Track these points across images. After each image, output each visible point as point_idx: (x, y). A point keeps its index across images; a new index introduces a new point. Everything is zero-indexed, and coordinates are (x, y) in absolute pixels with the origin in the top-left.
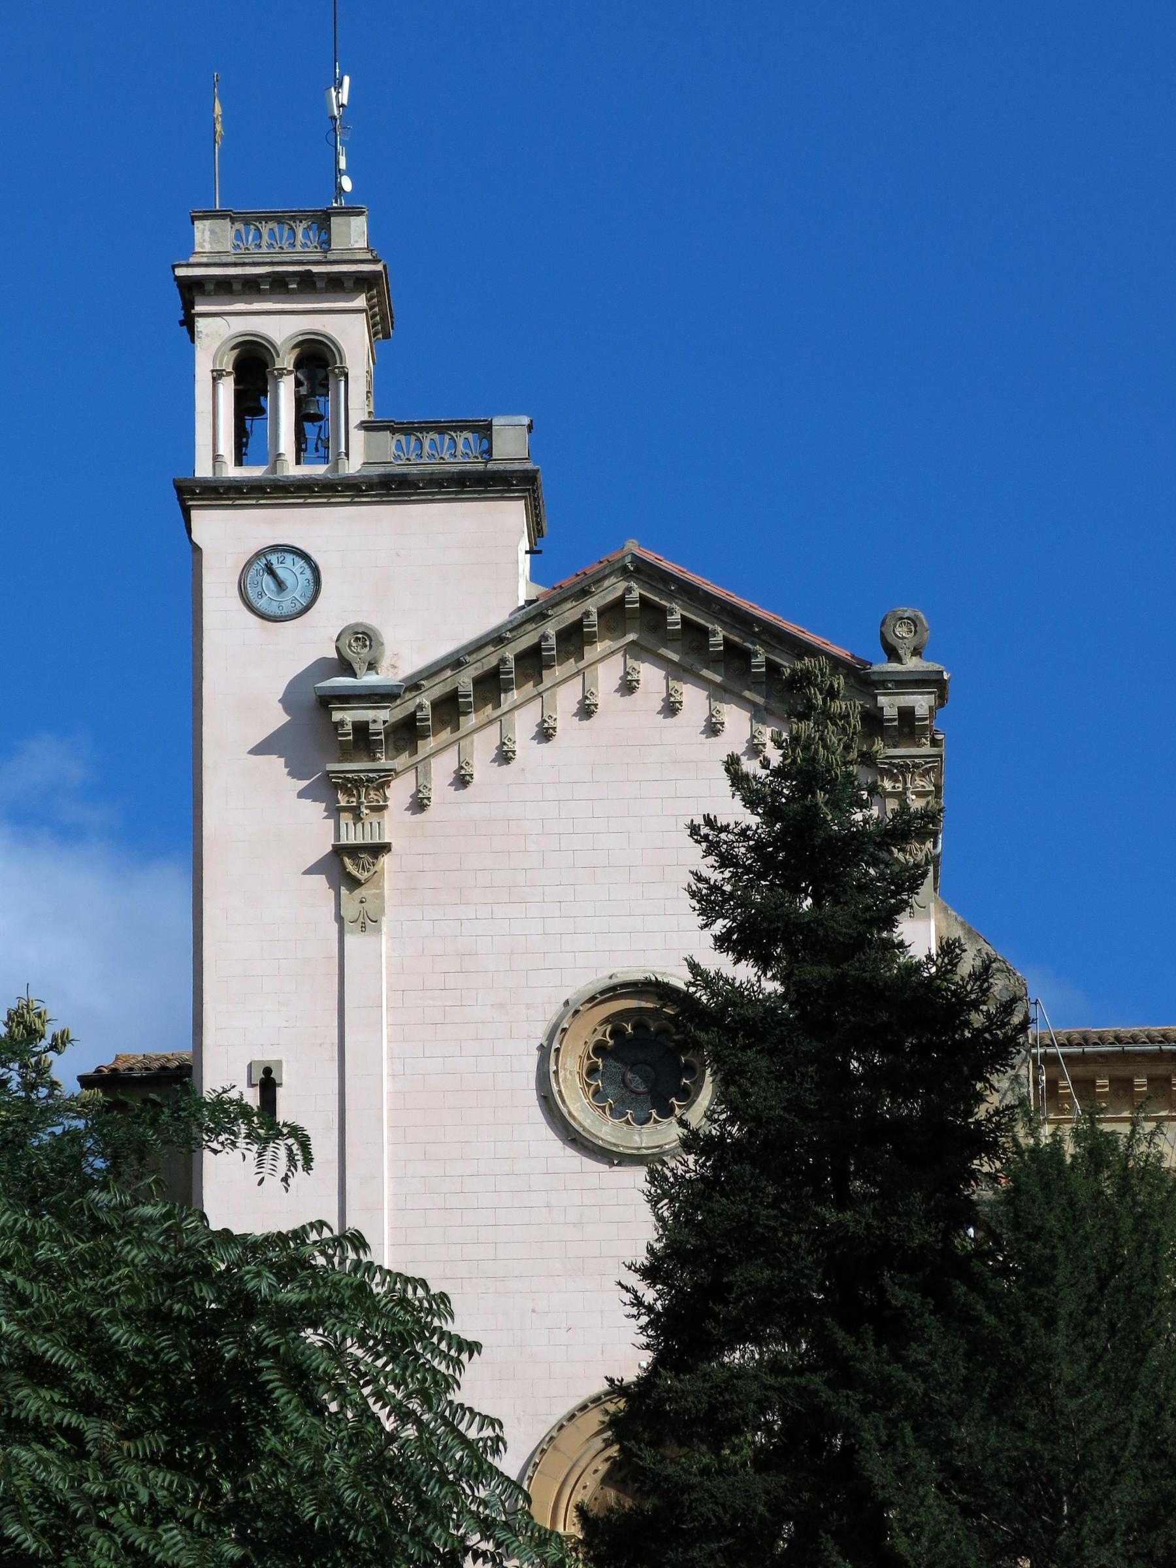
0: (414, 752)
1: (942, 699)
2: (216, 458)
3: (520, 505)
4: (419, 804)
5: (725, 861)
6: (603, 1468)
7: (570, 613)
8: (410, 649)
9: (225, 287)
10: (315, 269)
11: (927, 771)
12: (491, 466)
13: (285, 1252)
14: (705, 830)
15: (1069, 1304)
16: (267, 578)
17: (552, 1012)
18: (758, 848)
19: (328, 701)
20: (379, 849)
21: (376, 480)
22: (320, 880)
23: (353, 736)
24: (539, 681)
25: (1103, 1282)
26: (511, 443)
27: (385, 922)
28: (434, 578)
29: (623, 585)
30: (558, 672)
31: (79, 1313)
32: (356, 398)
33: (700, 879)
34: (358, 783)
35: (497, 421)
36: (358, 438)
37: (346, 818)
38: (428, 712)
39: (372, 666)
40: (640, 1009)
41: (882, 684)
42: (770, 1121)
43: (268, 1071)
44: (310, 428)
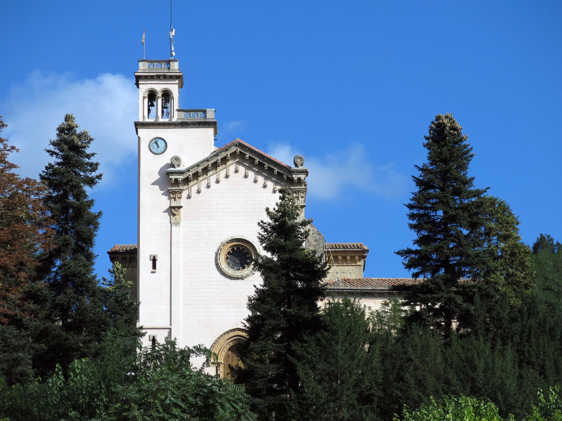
0: (188, 185)
1: (307, 175)
2: (144, 117)
4: (189, 197)
5: (266, 230)
6: (228, 347)
7: (224, 154)
8: (187, 162)
9: (146, 78)
10: (167, 74)
11: (303, 192)
12: (206, 120)
14: (261, 224)
15: (341, 338)
16: (155, 145)
17: (218, 245)
18: (272, 227)
19: (168, 174)
20: (180, 207)
22: (167, 214)
23: (174, 181)
24: (216, 169)
25: (348, 334)
26: (211, 115)
27: (181, 224)
28: (193, 146)
29: (236, 148)
30: (221, 167)
31: (183, 395)
32: (176, 103)
33: (260, 234)
34: (175, 192)
35: (208, 110)
36: (176, 113)
37: (172, 200)
38: (191, 176)
39: (179, 166)
40: (238, 245)
42: (275, 288)
43: (154, 257)
44: (165, 110)
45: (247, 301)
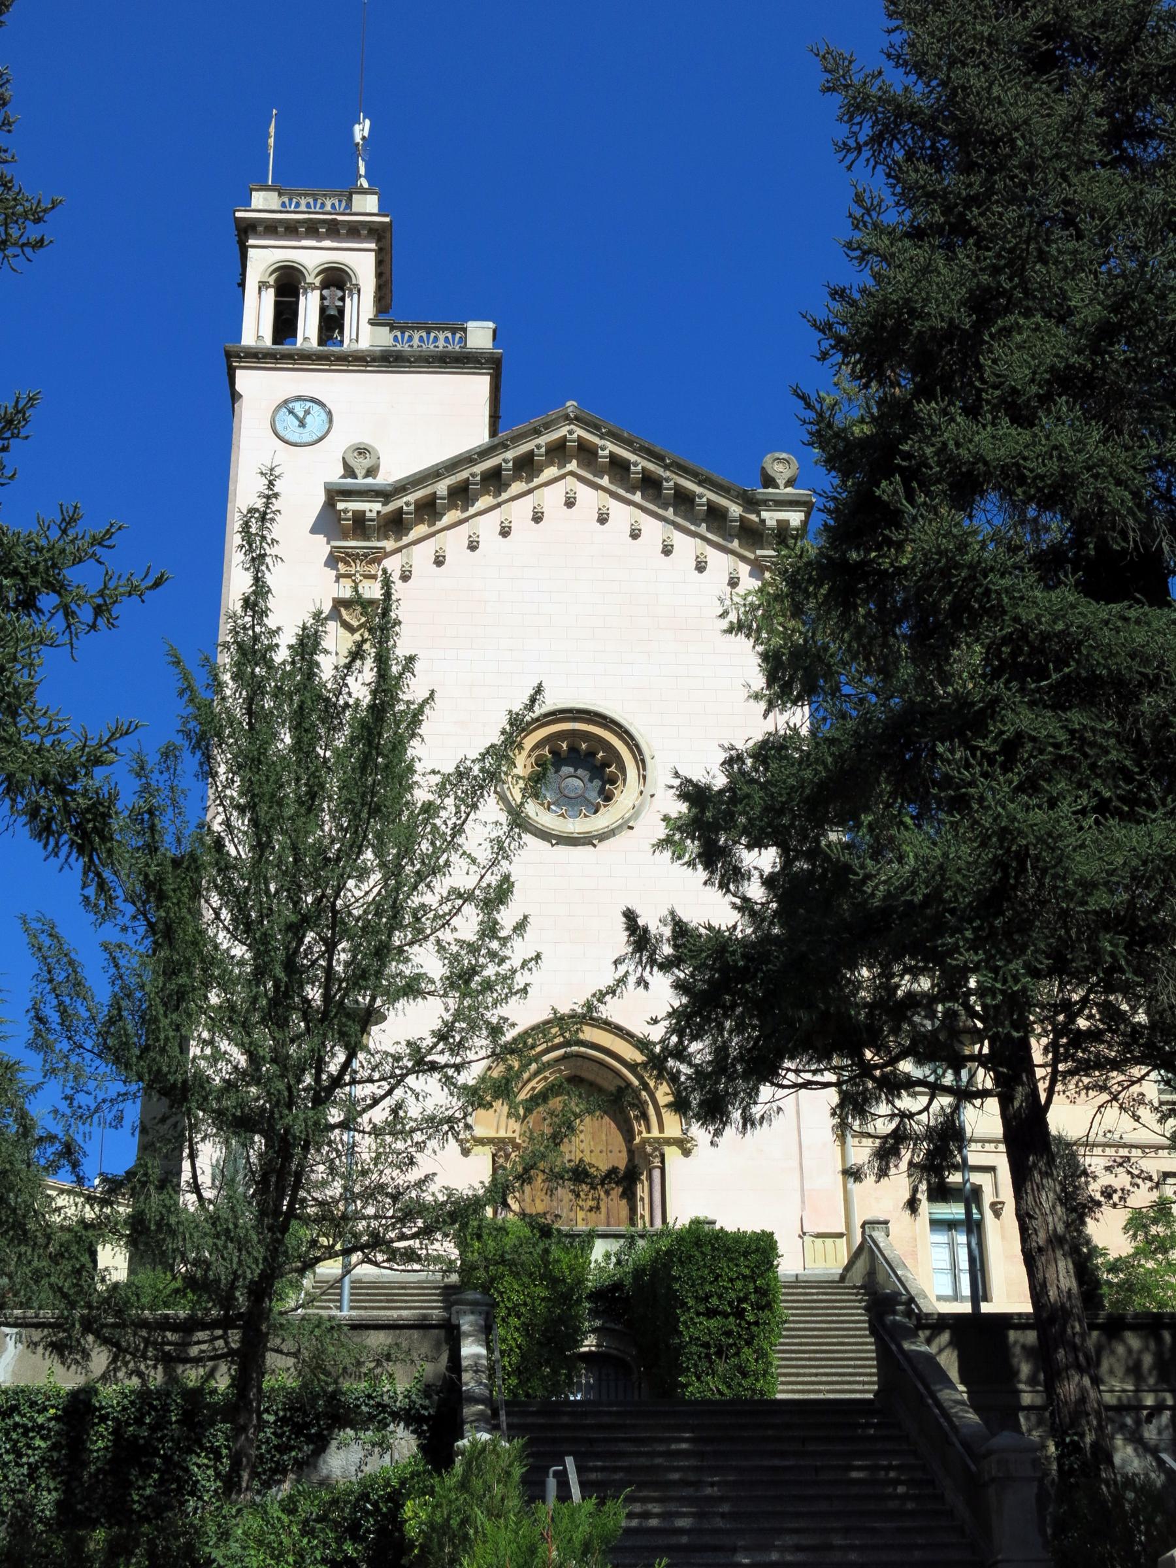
9: (272, 229)
30: (517, 487)
40: (574, 732)
41: (765, 502)
45: (768, 1230)
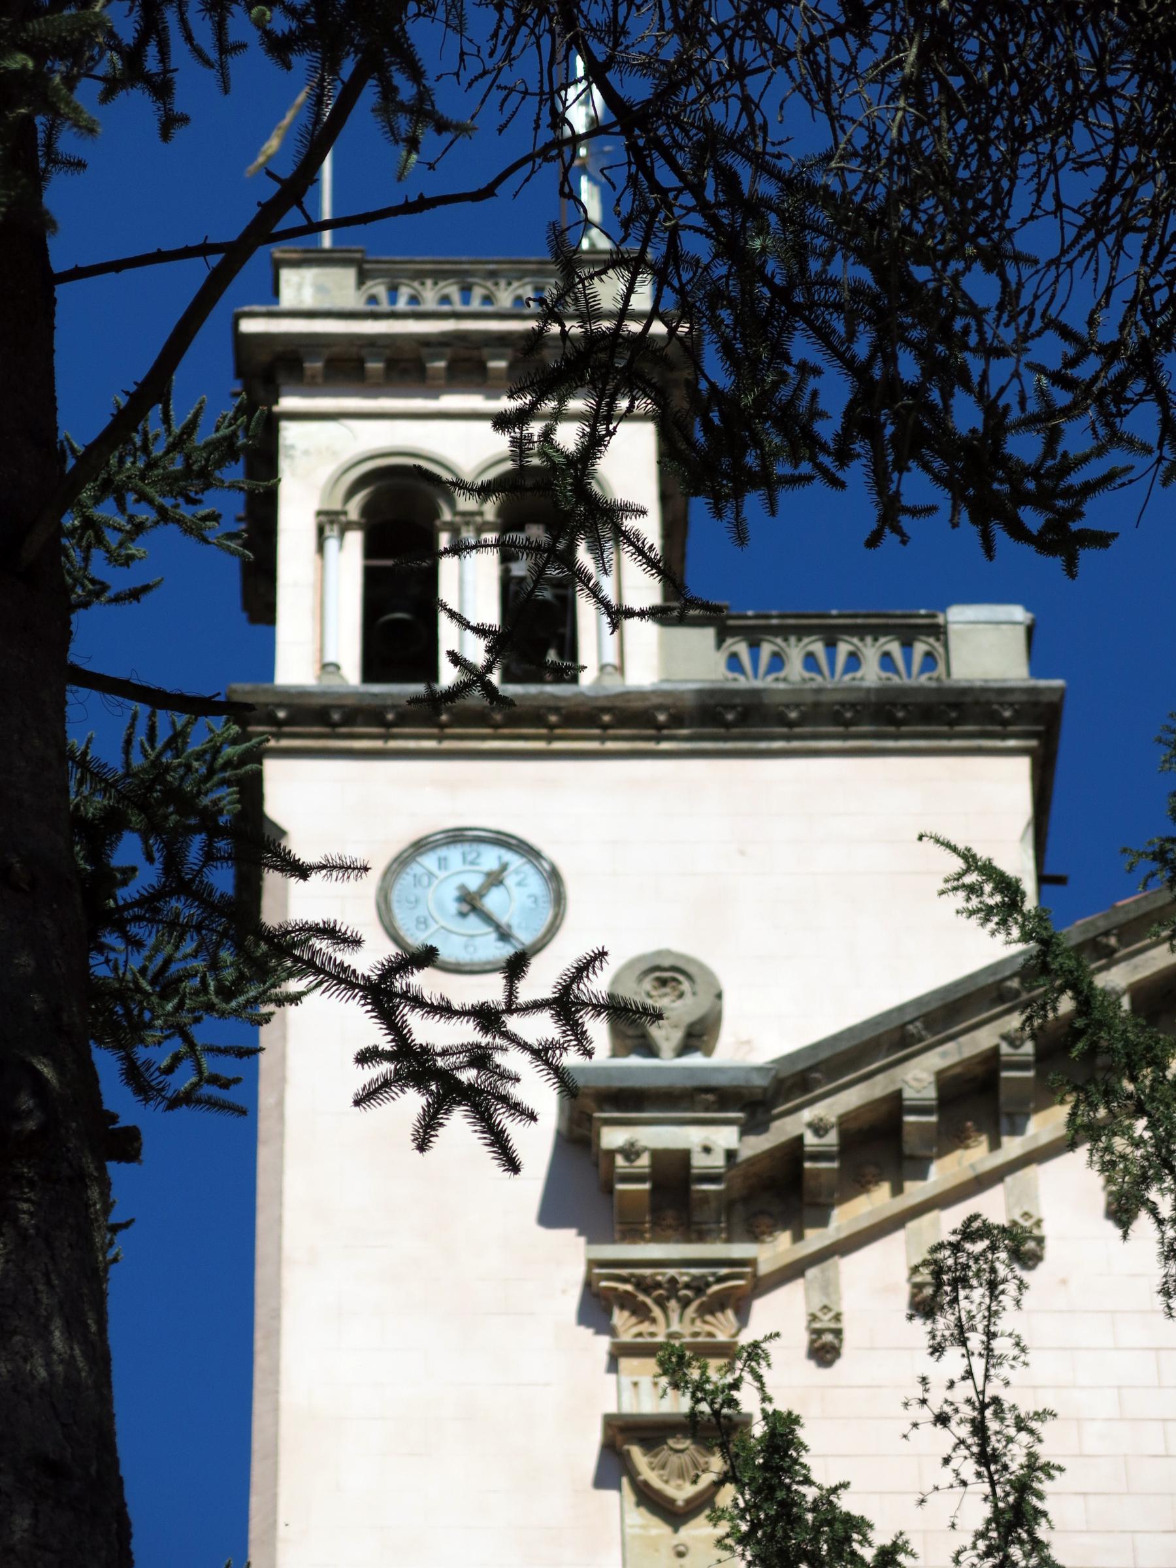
3: (1021, 767)
13: (1081, 531)
21: (690, 702)
